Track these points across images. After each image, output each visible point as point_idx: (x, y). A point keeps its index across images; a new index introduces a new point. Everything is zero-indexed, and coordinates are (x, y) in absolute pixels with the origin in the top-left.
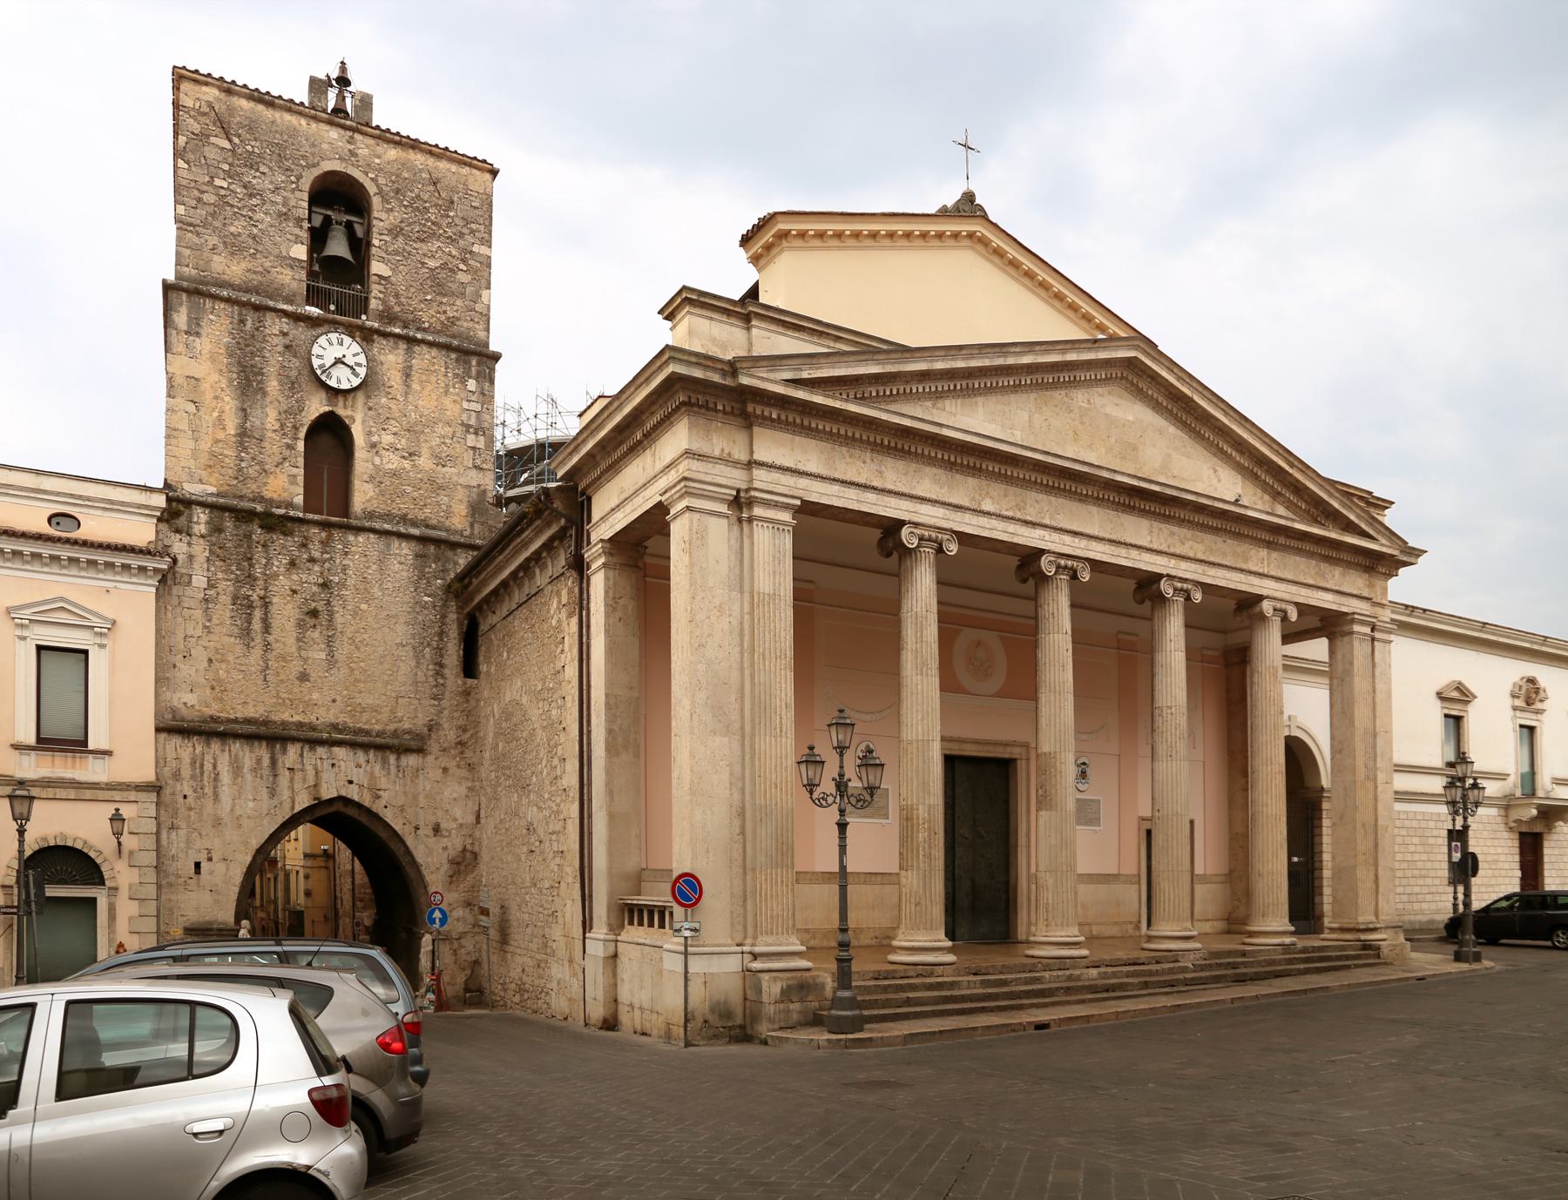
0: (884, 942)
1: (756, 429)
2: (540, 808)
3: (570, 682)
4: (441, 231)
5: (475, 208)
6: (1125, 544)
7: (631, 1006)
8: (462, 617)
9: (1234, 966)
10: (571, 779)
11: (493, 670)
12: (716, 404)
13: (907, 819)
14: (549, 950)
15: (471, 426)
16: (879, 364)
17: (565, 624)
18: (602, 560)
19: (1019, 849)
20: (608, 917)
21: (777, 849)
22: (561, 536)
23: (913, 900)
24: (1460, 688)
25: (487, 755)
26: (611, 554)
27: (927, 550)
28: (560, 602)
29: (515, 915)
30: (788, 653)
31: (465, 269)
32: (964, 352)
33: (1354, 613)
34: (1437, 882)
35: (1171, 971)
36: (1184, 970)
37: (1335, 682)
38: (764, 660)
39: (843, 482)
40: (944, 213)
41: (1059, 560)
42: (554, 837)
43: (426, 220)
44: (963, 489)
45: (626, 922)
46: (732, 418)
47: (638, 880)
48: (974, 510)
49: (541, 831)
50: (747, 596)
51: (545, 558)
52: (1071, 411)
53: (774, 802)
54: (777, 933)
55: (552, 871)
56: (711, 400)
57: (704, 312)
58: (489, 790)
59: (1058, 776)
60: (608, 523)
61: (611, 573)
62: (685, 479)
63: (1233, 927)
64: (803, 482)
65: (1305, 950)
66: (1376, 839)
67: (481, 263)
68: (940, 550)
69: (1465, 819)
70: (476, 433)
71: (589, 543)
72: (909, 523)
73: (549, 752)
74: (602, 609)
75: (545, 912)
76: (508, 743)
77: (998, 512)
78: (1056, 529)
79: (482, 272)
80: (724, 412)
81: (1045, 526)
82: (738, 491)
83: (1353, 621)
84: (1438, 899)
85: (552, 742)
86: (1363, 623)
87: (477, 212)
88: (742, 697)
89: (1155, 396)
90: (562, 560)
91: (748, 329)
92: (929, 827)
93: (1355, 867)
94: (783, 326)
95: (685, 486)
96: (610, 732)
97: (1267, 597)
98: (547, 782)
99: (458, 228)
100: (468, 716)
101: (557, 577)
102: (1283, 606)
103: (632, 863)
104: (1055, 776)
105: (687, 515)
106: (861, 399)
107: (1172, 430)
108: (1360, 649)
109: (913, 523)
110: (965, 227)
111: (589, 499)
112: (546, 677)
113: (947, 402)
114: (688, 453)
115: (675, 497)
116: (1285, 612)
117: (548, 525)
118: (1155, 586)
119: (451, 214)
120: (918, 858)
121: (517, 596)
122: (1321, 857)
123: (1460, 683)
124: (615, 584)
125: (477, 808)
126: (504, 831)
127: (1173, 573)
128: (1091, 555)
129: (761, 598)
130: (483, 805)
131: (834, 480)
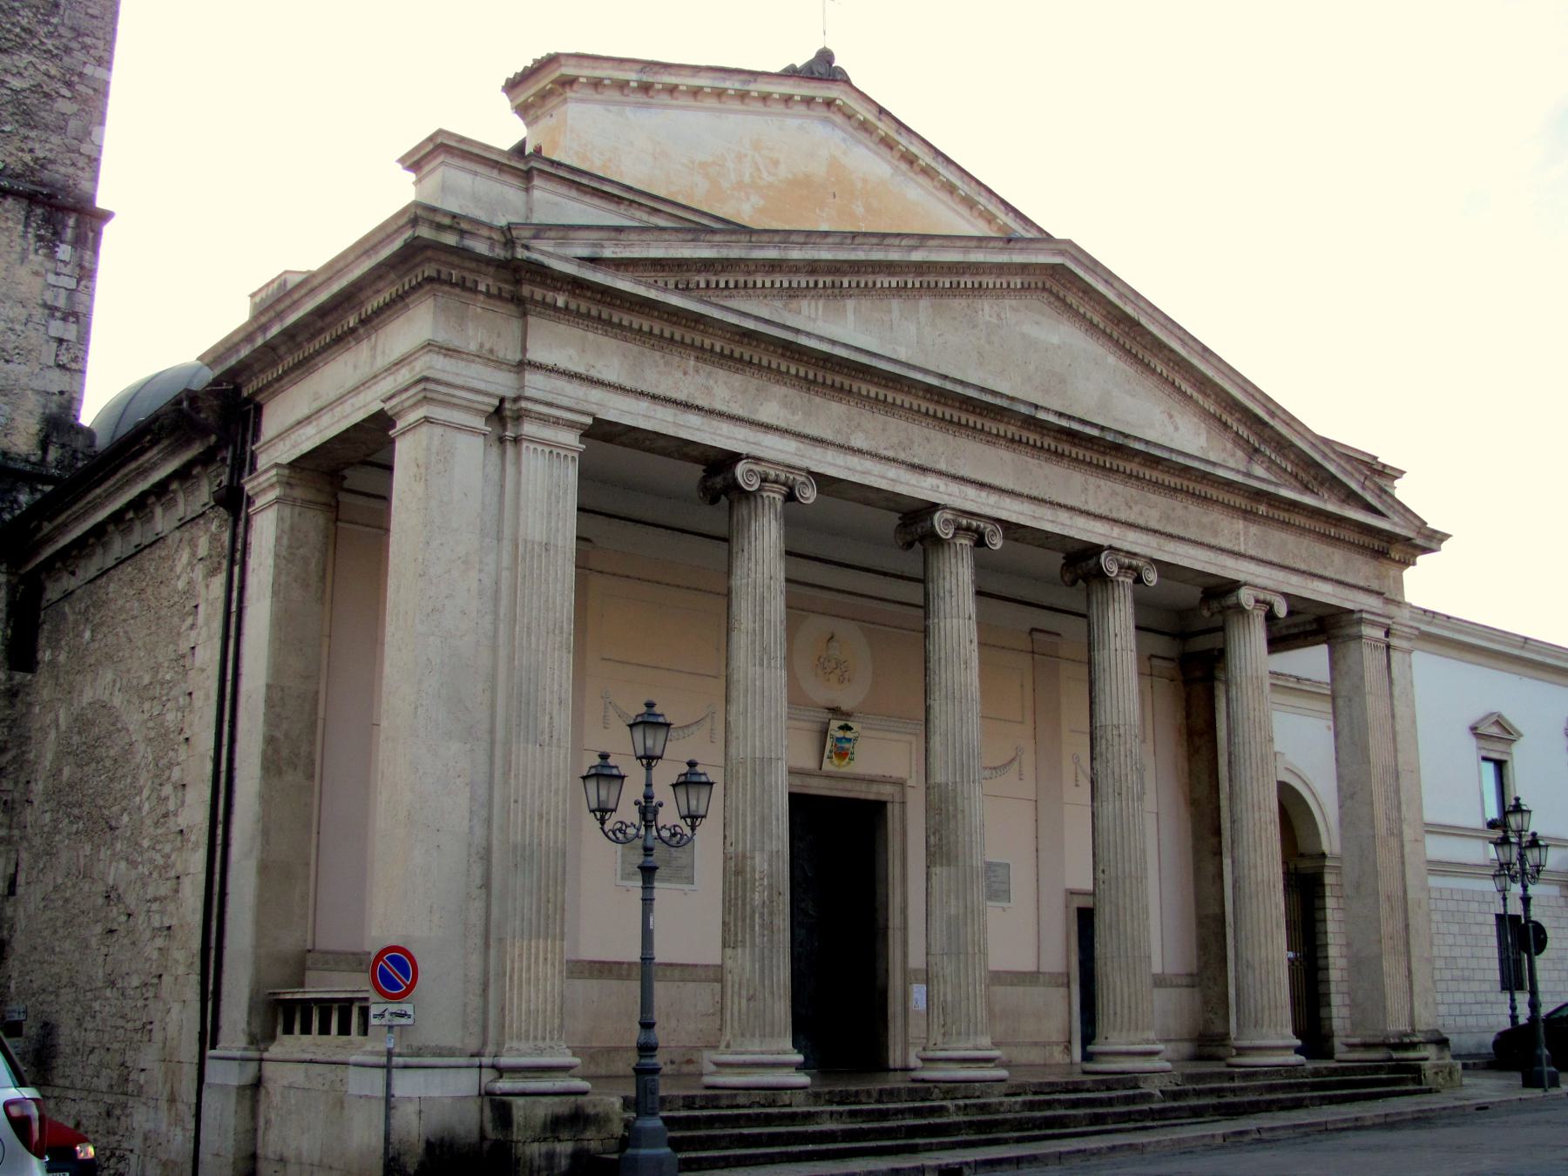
0: (686, 1069)
1: (531, 320)
2: (133, 864)
3: (203, 670)
4: (36, 42)
5: (92, 16)
6: (1051, 503)
7: (282, 1160)
8: (15, 580)
9: (1218, 1092)
10: (195, 813)
11: (62, 658)
12: (476, 282)
13: (737, 873)
14: (131, 1087)
15: (56, 309)
16: (712, 247)
17: (200, 588)
18: (272, 495)
19: (890, 932)
20: (249, 1023)
21: (539, 911)
22: (206, 459)
23: (744, 992)
24: (1500, 722)
25: (38, 787)
26: (289, 484)
27: (772, 495)
28: (194, 554)
29: (67, 1034)
30: (565, 626)
31: (68, 94)
32: (830, 240)
33: (1361, 611)
34: (1486, 987)
35: (1128, 1100)
36: (1148, 1097)
37: (1340, 702)
38: (529, 634)
39: (654, 397)
40: (791, 73)
41: (960, 520)
42: (155, 906)
43: (13, 24)
44: (828, 417)
45: (280, 1029)
46: (499, 303)
47: (300, 965)
48: (841, 446)
49: (131, 900)
50: (507, 545)
51: (174, 492)
52: (974, 327)
53: (536, 841)
54: (535, 1038)
55: (148, 959)
56: (469, 277)
57: (467, 164)
58: (37, 841)
59: (960, 816)
60: (288, 443)
61: (287, 511)
62: (426, 379)
63: (1207, 1050)
64: (596, 394)
65: (1316, 1073)
66: (1406, 918)
67: (95, 90)
68: (790, 497)
69: (1525, 888)
70: (65, 319)
71: (253, 468)
72: (748, 457)
73: (157, 776)
74: (270, 561)
75: (130, 1026)
76: (80, 766)
77: (873, 450)
78: (955, 478)
79: (93, 101)
80: (488, 294)
81: (940, 473)
82: (502, 400)
83: (1360, 621)
84: (1489, 1011)
85: (164, 762)
86: (1373, 624)
87: (95, 22)
88: (493, 689)
89: (1089, 315)
90: (204, 493)
91: (527, 190)
92: (771, 886)
93: (1379, 957)
94: (578, 189)
95: (425, 389)
96: (270, 741)
97: (1245, 584)
98: (148, 822)
99: (64, 40)
100: (10, 728)
101: (193, 519)
102: (1269, 597)
103: (290, 942)
104: (955, 816)
105: (425, 428)
106: (685, 290)
107: (1111, 359)
108: (1372, 661)
109: (754, 458)
110: (820, 91)
111: (259, 409)
112: (160, 665)
113: (804, 303)
114: (429, 346)
115: (406, 404)
116: (1271, 606)
117: (188, 443)
118: (1092, 562)
119: (55, 20)
120: (753, 929)
121: (119, 547)
122: (1326, 951)
123: (1500, 716)
124: (292, 528)
125: (11, 870)
126: (60, 903)
127: (1117, 544)
128: (1004, 515)
129: (529, 548)
130: (23, 865)
131: (642, 393)
